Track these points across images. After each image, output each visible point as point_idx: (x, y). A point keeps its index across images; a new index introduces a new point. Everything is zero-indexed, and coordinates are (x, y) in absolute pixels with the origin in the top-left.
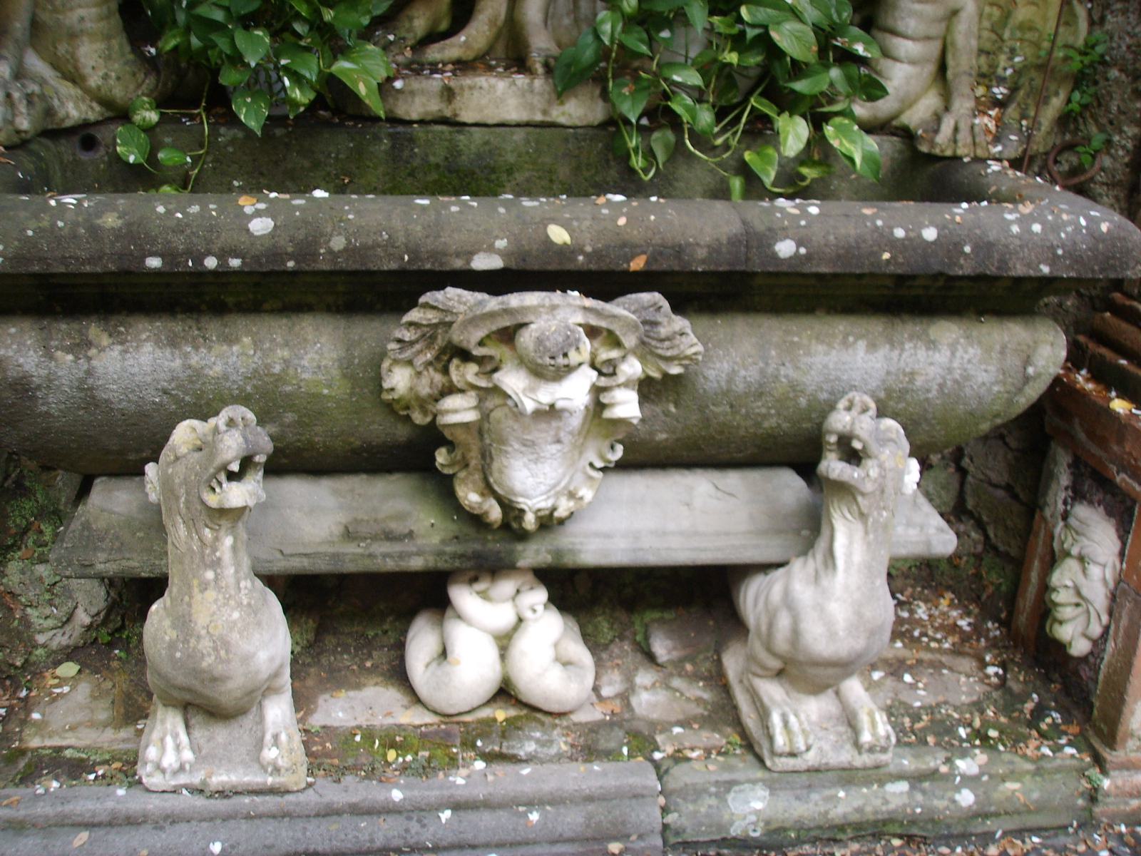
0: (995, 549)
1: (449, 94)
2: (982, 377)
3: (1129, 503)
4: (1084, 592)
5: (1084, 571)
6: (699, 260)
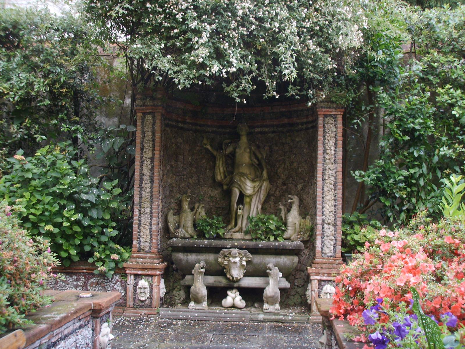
1: (232, 235)
6: (251, 247)
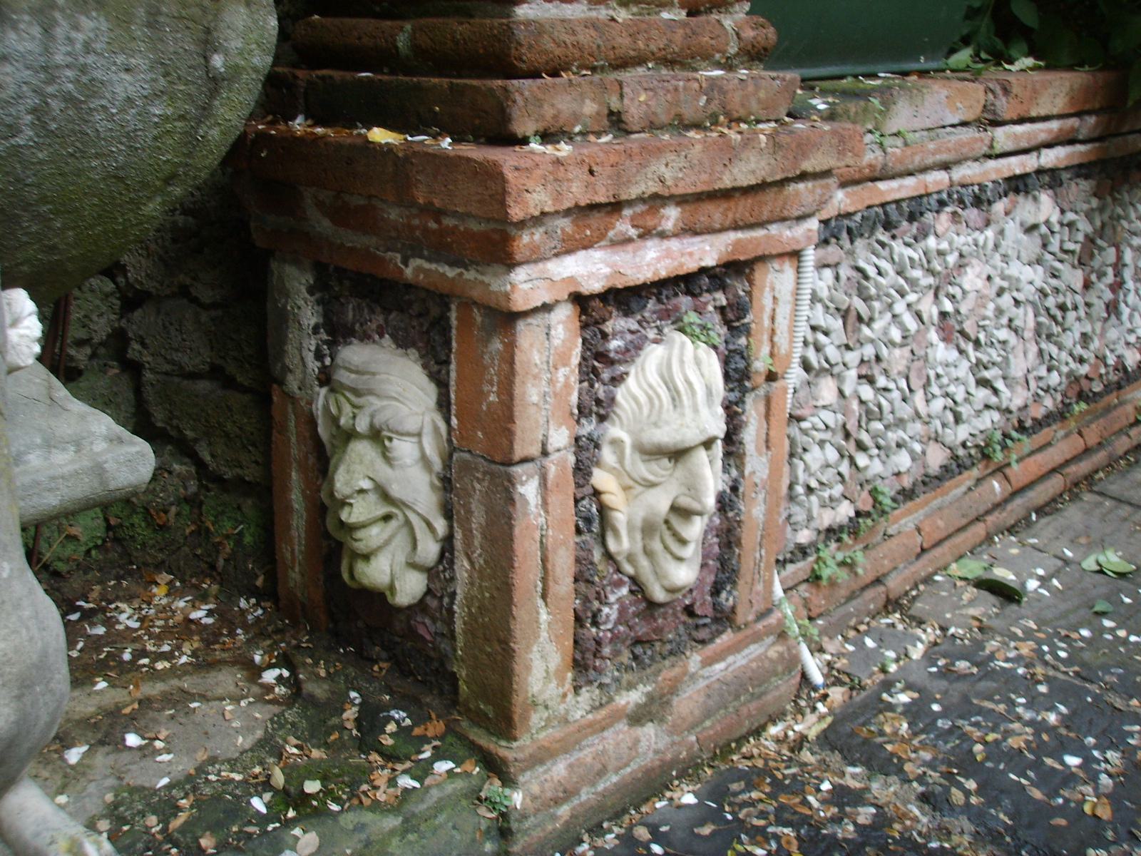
0: (219, 480)
2: (124, 85)
3: (435, 311)
4: (396, 491)
5: (386, 455)
